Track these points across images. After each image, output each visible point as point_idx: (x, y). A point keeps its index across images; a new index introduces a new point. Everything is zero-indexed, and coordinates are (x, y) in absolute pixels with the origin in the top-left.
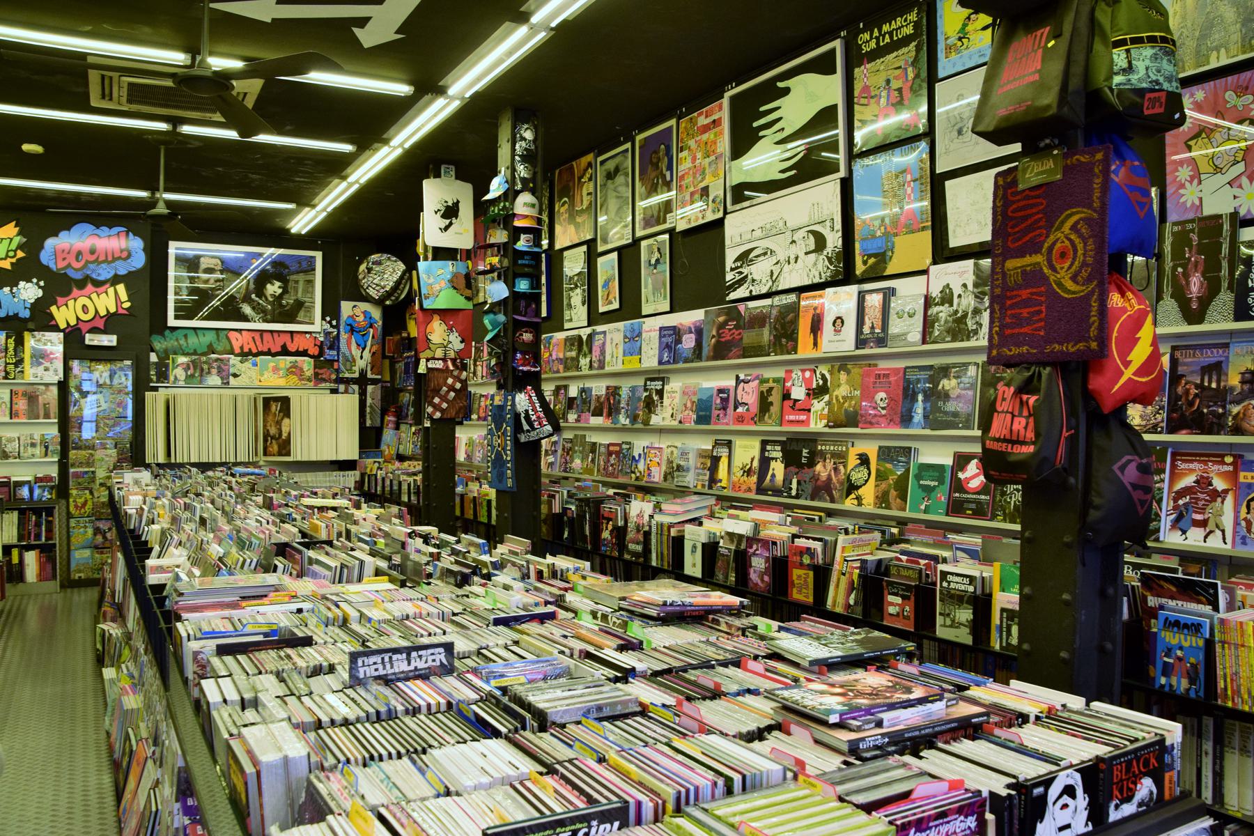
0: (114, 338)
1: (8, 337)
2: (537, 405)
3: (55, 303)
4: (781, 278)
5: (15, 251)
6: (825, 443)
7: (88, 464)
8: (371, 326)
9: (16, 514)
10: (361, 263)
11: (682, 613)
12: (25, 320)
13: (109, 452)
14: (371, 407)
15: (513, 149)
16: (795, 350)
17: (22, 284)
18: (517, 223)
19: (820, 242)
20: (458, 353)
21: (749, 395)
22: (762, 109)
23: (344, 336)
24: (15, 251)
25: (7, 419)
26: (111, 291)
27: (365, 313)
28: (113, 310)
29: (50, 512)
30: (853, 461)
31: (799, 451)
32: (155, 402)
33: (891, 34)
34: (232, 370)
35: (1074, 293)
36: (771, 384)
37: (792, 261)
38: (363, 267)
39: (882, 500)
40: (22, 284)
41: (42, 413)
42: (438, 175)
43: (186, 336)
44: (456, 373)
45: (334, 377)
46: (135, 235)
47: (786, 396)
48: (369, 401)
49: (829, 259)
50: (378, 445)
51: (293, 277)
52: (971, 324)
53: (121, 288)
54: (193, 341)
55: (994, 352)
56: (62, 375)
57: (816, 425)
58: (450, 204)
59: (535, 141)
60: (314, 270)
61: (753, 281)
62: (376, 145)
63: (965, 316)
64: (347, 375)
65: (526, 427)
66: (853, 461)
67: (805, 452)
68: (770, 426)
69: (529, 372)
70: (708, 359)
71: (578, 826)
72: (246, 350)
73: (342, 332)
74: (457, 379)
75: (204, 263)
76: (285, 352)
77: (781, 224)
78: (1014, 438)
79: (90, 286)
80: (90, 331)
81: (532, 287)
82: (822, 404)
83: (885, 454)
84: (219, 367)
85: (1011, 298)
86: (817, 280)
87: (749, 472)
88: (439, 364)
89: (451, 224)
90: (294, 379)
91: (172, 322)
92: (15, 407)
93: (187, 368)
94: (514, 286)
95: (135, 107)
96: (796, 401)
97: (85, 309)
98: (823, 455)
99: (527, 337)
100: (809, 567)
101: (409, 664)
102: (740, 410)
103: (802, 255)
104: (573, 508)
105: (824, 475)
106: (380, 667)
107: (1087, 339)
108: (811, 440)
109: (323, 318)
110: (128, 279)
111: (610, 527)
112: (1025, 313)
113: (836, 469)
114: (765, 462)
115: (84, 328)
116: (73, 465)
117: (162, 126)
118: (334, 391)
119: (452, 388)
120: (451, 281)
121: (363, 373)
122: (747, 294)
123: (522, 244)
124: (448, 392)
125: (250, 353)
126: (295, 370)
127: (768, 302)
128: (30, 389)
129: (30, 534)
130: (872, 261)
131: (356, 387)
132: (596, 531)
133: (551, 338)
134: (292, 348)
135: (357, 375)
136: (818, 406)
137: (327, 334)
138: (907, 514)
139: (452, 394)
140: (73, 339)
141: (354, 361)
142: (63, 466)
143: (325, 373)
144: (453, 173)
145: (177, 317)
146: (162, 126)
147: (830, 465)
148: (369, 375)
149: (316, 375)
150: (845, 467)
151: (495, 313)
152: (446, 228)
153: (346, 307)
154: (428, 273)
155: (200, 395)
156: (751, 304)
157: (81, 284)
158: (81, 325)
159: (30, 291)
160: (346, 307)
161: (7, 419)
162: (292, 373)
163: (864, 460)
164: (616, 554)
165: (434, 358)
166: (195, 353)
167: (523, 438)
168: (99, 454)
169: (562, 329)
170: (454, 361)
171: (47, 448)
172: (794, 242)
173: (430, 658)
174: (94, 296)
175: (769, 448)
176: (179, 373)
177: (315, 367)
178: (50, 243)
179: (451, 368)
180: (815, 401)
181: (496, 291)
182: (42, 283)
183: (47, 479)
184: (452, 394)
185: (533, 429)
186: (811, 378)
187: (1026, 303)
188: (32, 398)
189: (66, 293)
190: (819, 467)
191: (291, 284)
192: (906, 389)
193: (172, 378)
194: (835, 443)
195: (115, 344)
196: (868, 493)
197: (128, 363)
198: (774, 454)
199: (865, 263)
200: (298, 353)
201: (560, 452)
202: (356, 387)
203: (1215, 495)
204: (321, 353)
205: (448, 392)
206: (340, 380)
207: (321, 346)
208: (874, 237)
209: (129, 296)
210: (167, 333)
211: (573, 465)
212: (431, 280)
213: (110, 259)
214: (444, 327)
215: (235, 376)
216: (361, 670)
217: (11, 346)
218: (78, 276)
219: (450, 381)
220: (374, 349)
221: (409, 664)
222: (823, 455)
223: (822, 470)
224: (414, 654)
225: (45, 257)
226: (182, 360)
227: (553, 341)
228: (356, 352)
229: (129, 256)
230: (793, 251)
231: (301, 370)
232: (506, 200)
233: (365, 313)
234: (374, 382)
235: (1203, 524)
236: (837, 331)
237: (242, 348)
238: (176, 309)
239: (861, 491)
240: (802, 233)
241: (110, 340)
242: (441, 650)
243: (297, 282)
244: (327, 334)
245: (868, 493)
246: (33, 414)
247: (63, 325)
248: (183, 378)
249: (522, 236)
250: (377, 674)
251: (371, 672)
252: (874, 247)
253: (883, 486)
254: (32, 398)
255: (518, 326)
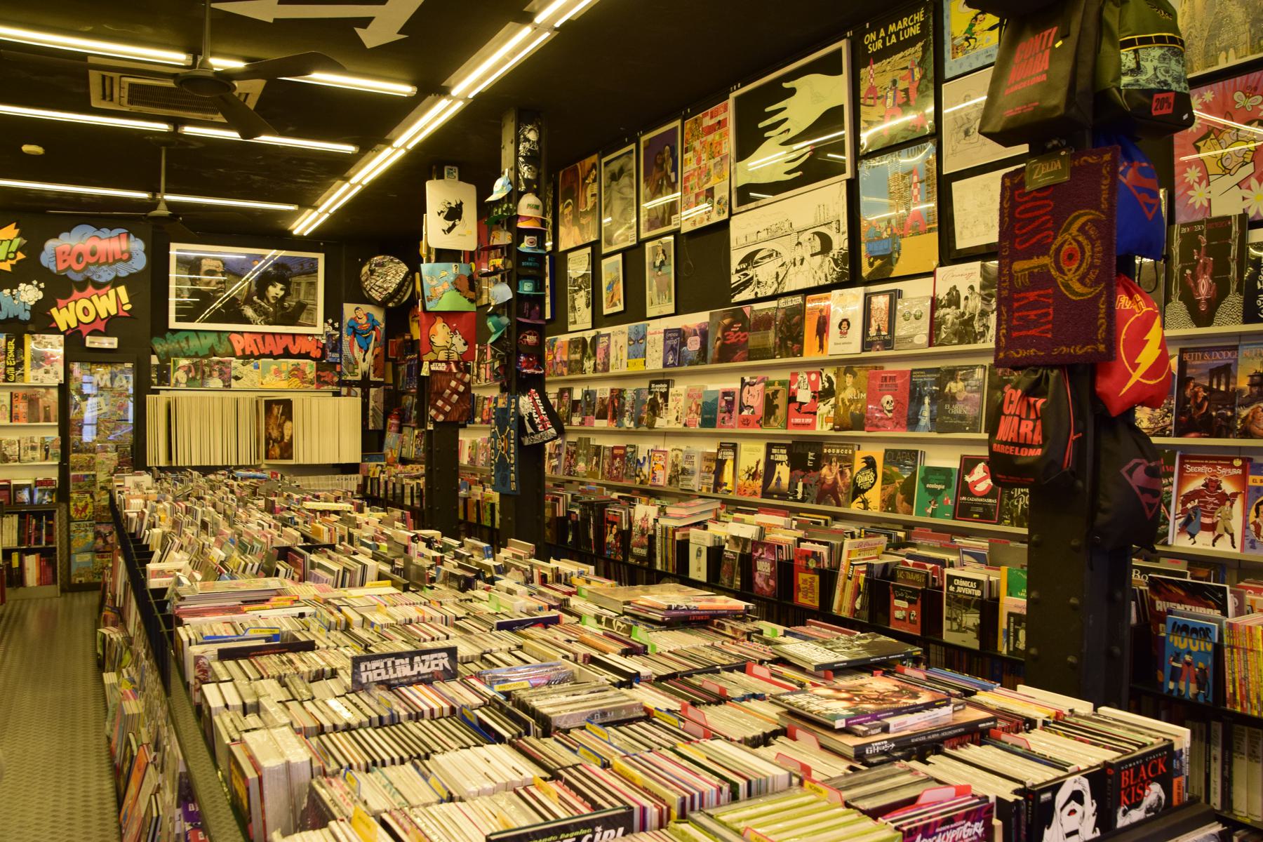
0: (115, 340)
1: (8, 340)
2: (541, 408)
3: (55, 305)
4: (787, 280)
5: (15, 253)
6: (831, 446)
7: (89, 468)
8: (374, 329)
9: (16, 518)
10: (363, 265)
11: (688, 617)
12: (25, 323)
13: (110, 455)
14: (374, 409)
15: (517, 150)
16: (801, 353)
17: (22, 286)
18: (521, 225)
19: (826, 243)
20: (462, 355)
21: (754, 397)
22: (768, 110)
23: (346, 339)
24: (15, 253)
25: (7, 422)
26: (112, 293)
27: (368, 315)
28: (113, 312)
29: (50, 515)
30: (859, 464)
31: (805, 454)
32: (156, 404)
33: (897, 34)
34: (233, 373)
35: (1082, 295)
36: (777, 387)
37: (798, 263)
38: (365, 269)
39: (889, 503)
40: (22, 286)
41: (42, 416)
42: (441, 177)
43: (187, 339)
44: (459, 376)
45: (336, 379)
46: (136, 236)
47: (792, 399)
48: (372, 404)
49: (835, 261)
50: (381, 448)
51: (295, 279)
52: (977, 327)
53: (122, 290)
54: (194, 343)
55: (1002, 355)
56: (62, 378)
57: (822, 428)
58: (453, 205)
59: (539, 142)
60: (316, 271)
61: (759, 283)
62: (379, 146)
63: (972, 318)
64: (349, 378)
65: (530, 430)
66: (859, 464)
67: (811, 455)
68: (775, 429)
69: (533, 374)
70: (713, 362)
71: (583, 832)
72: (248, 352)
73: (345, 335)
74: (460, 381)
75: (206, 265)
76: (287, 354)
77: (787, 225)
78: (1022, 441)
79: (90, 288)
80: (91, 334)
81: (536, 289)
82: (828, 407)
83: (891, 457)
84: (221, 370)
85: (1018, 300)
86: (823, 282)
87: (754, 476)
88: (443, 367)
89: (454, 225)
90: (296, 381)
91: (173, 324)
92: (15, 410)
93: (188, 371)
94: (518, 288)
95: (135, 108)
96: (802, 404)
97: (86, 311)
98: (828, 458)
99: (531, 339)
100: (815, 571)
101: (412, 669)
102: (745, 413)
103: (807, 257)
104: (578, 512)
105: (830, 479)
106: (383, 671)
107: (1095, 341)
108: (817, 443)
109: (326, 321)
110: (130, 281)
111: (614, 531)
112: (1032, 315)
113: (842, 473)
114: (770, 465)
115: (85, 330)
116: (74, 469)
117: (163, 127)
118: (337, 394)
119: (455, 391)
120: (454, 283)
121: (365, 375)
122: (752, 296)
123: (526, 246)
124: (451, 395)
125: (252, 356)
126: (297, 373)
127: (773, 304)
128: (30, 392)
129: (30, 537)
130: (878, 263)
131: (358, 390)
132: (601, 535)
133: (555, 340)
134: (294, 351)
135: (359, 378)
136: (824, 409)
137: (329, 336)
138: (914, 518)
139: (456, 397)
140: (74, 341)
141: (357, 363)
142: (64, 469)
143: (327, 375)
144: (456, 174)
145: (178, 320)
146: (163, 127)
147: (836, 468)
148: (372, 378)
149: (318, 377)
150: (851, 470)
151: (499, 316)
152: (450, 230)
153: (349, 310)
154: (432, 275)
155: (202, 398)
156: (757, 306)
157: (82, 286)
158: (82, 328)
159: (30, 294)
160: (349, 310)
161: (7, 422)
162: (294, 376)
163: (870, 463)
164: (620, 558)
165: (437, 361)
166: (196, 355)
167: (527, 442)
168: (100, 457)
169: (566, 331)
170: (457, 363)
171: (47, 451)
172: (799, 243)
173: (433, 663)
174: (95, 298)
175: (774, 451)
176: (181, 376)
177: (317, 370)
178: (51, 245)
179: (455, 370)
180: (821, 404)
181: (500, 293)
182: (42, 285)
183: (48, 482)
184: (456, 397)
185: (537, 432)
186: (817, 380)
187: (1033, 305)
188: (32, 401)
189: (67, 295)
190: (825, 471)
191: (293, 286)
192: (912, 393)
193: (173, 381)
194: (841, 446)
195: (115, 346)
196: (874, 496)
197: (129, 365)
198: (780, 458)
199: (871, 265)
200: (300, 356)
201: (564, 455)
202: (358, 390)
203: (1224, 498)
204: (324, 356)
205: (451, 395)
206: (342, 383)
207: (323, 349)
208: (880, 238)
209: (130, 298)
210: (168, 335)
211: (578, 468)
212: (435, 283)
213: (111, 260)
214: (447, 329)
215: (237, 378)
216: (364, 675)
217: (11, 348)
218: (79, 278)
219: (453, 384)
220: (377, 352)
221: (412, 669)
222: (828, 458)
223: (828, 473)
224: (417, 659)
225: (46, 259)
226: (183, 362)
227: (557, 344)
228: (358, 354)
229: (130, 258)
230: (799, 253)
231: (304, 372)
232: (509, 201)
233: (368, 315)
234: (377, 385)
235: (1211, 528)
236: (843, 334)
237: (243, 350)
238: (178, 311)
239: (867, 495)
240: (808, 234)
241: (110, 343)
242: (444, 655)
243: (299, 284)
244: (329, 336)
245: (874, 496)
246: (33, 417)
247: (63, 328)
248: (184, 380)
249: (526, 238)
250: (379, 678)
251: (373, 676)
252: (880, 249)
253: (890, 489)
254: (32, 401)
255: (522, 328)
